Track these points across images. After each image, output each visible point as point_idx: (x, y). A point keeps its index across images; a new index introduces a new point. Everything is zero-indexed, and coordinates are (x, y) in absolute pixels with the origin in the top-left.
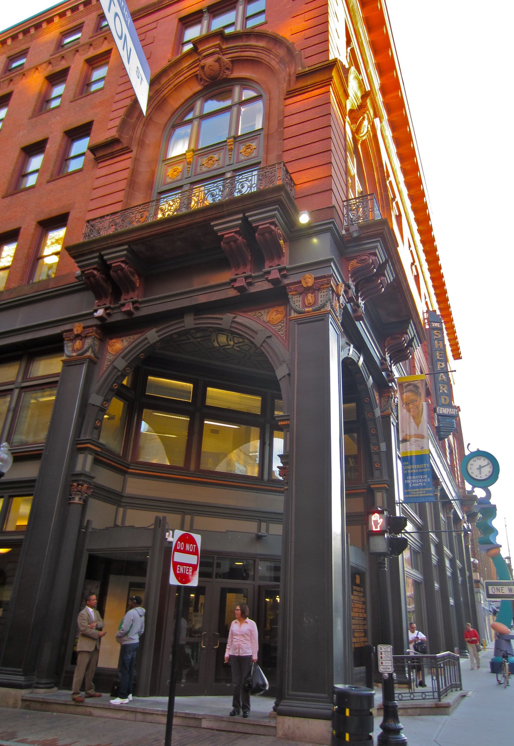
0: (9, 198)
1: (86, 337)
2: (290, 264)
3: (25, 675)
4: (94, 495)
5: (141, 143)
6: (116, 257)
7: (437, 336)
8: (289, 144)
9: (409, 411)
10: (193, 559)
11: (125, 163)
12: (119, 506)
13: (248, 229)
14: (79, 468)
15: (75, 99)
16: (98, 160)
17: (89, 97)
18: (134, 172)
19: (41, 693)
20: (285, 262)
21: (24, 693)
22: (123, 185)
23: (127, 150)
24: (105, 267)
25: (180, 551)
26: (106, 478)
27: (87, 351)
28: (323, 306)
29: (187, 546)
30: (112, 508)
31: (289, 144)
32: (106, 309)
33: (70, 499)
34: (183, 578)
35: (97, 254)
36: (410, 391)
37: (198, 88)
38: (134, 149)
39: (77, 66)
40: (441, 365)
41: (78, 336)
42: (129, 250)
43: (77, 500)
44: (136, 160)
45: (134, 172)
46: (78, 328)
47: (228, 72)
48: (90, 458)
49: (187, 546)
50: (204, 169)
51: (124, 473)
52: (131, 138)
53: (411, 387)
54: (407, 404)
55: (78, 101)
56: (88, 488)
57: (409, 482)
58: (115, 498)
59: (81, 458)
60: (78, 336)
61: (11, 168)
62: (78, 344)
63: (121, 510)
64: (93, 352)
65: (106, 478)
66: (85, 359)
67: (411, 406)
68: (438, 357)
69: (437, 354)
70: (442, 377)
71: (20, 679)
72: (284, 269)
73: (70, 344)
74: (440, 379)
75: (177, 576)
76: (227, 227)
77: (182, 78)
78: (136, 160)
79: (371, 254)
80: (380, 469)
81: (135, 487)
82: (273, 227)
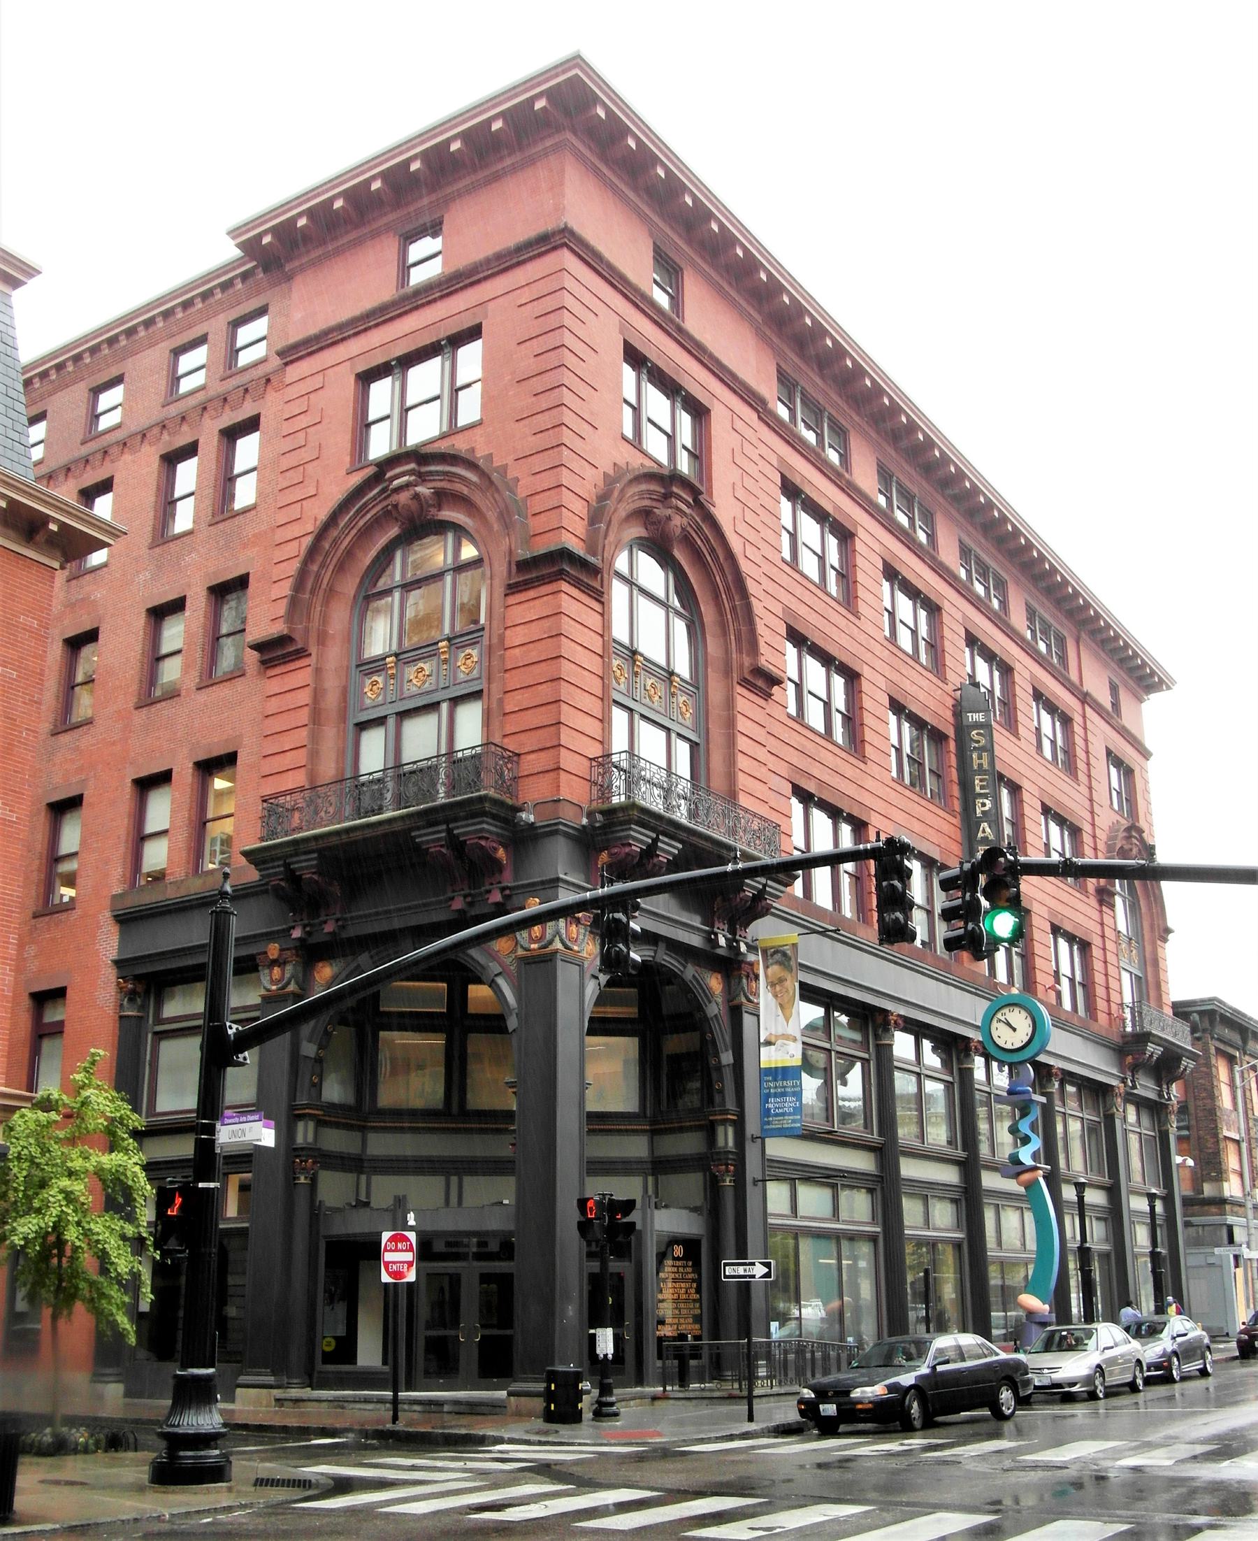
0: (145, 710)
1: (285, 963)
2: (516, 879)
3: (274, 1375)
4: (326, 1167)
5: (322, 638)
6: (306, 866)
7: (978, 742)
8: (514, 680)
9: (776, 996)
10: (409, 1256)
11: (300, 675)
12: (362, 1173)
13: (456, 845)
14: (300, 1139)
15: (217, 519)
16: (266, 664)
17: (236, 521)
18: (318, 695)
19: (294, 1393)
20: (508, 880)
21: (277, 1393)
22: (304, 716)
23: (302, 653)
24: (293, 878)
25: (391, 1251)
26: (337, 1141)
27: (288, 983)
28: (551, 942)
29: (399, 1245)
30: (350, 1178)
31: (514, 680)
32: (305, 926)
33: (295, 1179)
34: (397, 1275)
35: (281, 862)
36: (778, 963)
37: (394, 531)
38: (313, 650)
39: (209, 433)
40: (984, 805)
41: (274, 963)
42: (319, 858)
43: (302, 1180)
44: (318, 671)
45: (318, 695)
46: (273, 950)
47: (433, 511)
48: (311, 1125)
49: (399, 1245)
50: (414, 690)
51: (363, 1129)
52: (307, 630)
53: (778, 957)
54: (773, 985)
55: (221, 526)
56: (314, 1163)
57: (771, 1106)
58: (356, 1164)
59: (300, 1126)
60: (274, 963)
61: (138, 648)
62: (276, 971)
63: (363, 1178)
64: (297, 983)
65: (337, 1141)
66: (289, 994)
67: (778, 988)
68: (978, 789)
69: (977, 782)
70: (984, 831)
71: (271, 1379)
72: (508, 888)
73: (267, 971)
74: (980, 835)
75: (390, 1274)
76: (431, 838)
77: (369, 516)
78: (318, 671)
79: (623, 845)
80: (721, 1092)
81: (381, 1145)
82: (483, 843)
